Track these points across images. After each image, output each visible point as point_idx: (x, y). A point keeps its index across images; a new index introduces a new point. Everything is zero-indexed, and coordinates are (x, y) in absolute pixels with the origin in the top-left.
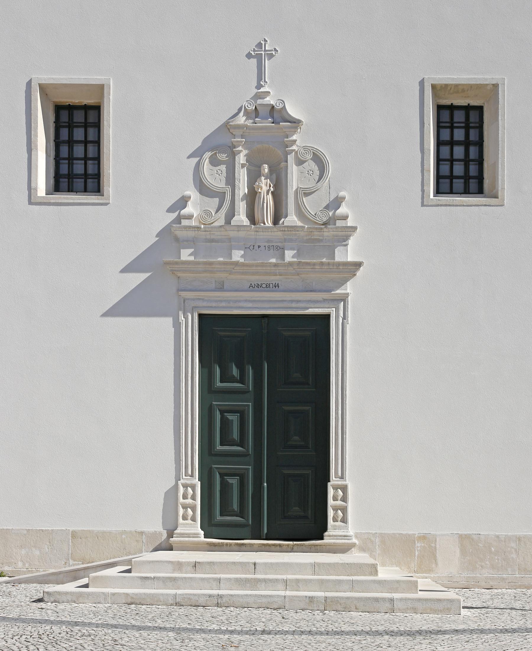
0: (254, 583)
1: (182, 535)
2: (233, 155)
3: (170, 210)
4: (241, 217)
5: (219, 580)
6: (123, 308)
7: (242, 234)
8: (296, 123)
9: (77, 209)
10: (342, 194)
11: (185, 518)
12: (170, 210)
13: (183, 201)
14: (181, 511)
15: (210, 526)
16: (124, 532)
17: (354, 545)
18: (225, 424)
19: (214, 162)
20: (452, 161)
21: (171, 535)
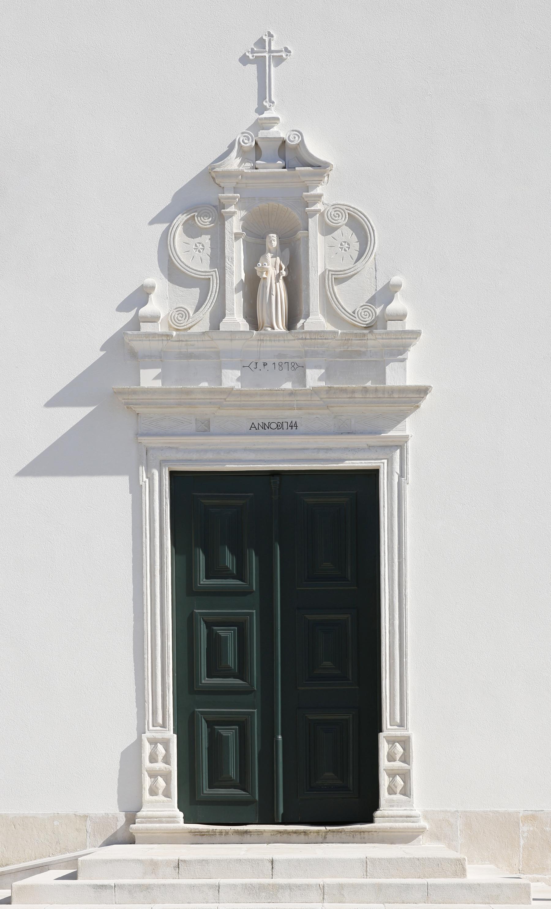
1: (149, 819)
2: (221, 220)
3: (123, 307)
4: (236, 319)
6: (54, 462)
8: (320, 167)
10: (395, 279)
11: (153, 792)
12: (123, 307)
13: (142, 295)
14: (147, 782)
17: (421, 831)
19: (192, 230)
21: (131, 819)
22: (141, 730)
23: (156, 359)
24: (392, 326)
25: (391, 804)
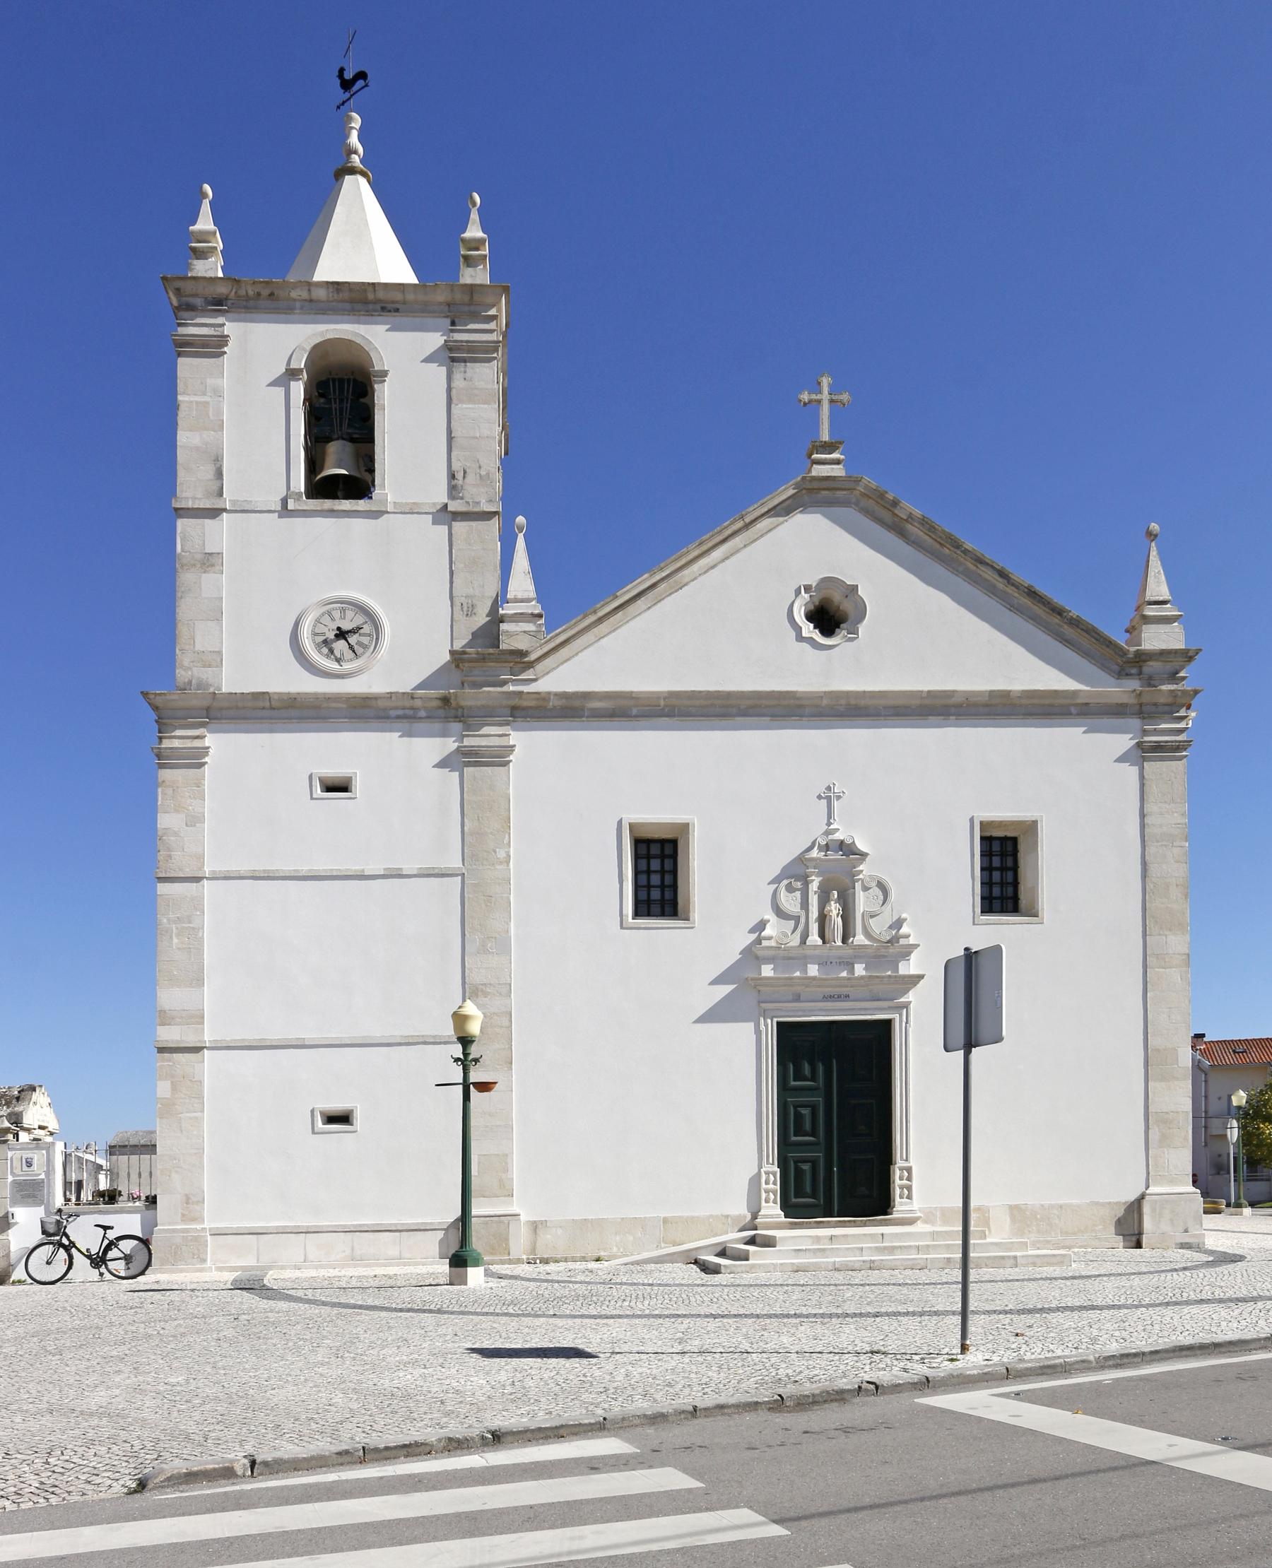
0: (892, 1250)
1: (766, 1216)
2: (806, 884)
3: (752, 931)
4: (814, 938)
5: (862, 1249)
6: (713, 1015)
7: (817, 952)
8: (864, 855)
9: (660, 931)
10: (904, 916)
11: (767, 1201)
12: (752, 931)
13: (762, 925)
14: (764, 1195)
15: (790, 1208)
16: (711, 1216)
17: (917, 1219)
18: (798, 1117)
19: (790, 889)
20: (649, 886)
21: (755, 1216)
22: (760, 1167)
23: (768, 960)
24: (902, 941)
25: (901, 1204)
